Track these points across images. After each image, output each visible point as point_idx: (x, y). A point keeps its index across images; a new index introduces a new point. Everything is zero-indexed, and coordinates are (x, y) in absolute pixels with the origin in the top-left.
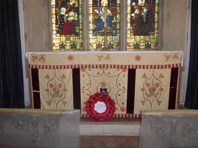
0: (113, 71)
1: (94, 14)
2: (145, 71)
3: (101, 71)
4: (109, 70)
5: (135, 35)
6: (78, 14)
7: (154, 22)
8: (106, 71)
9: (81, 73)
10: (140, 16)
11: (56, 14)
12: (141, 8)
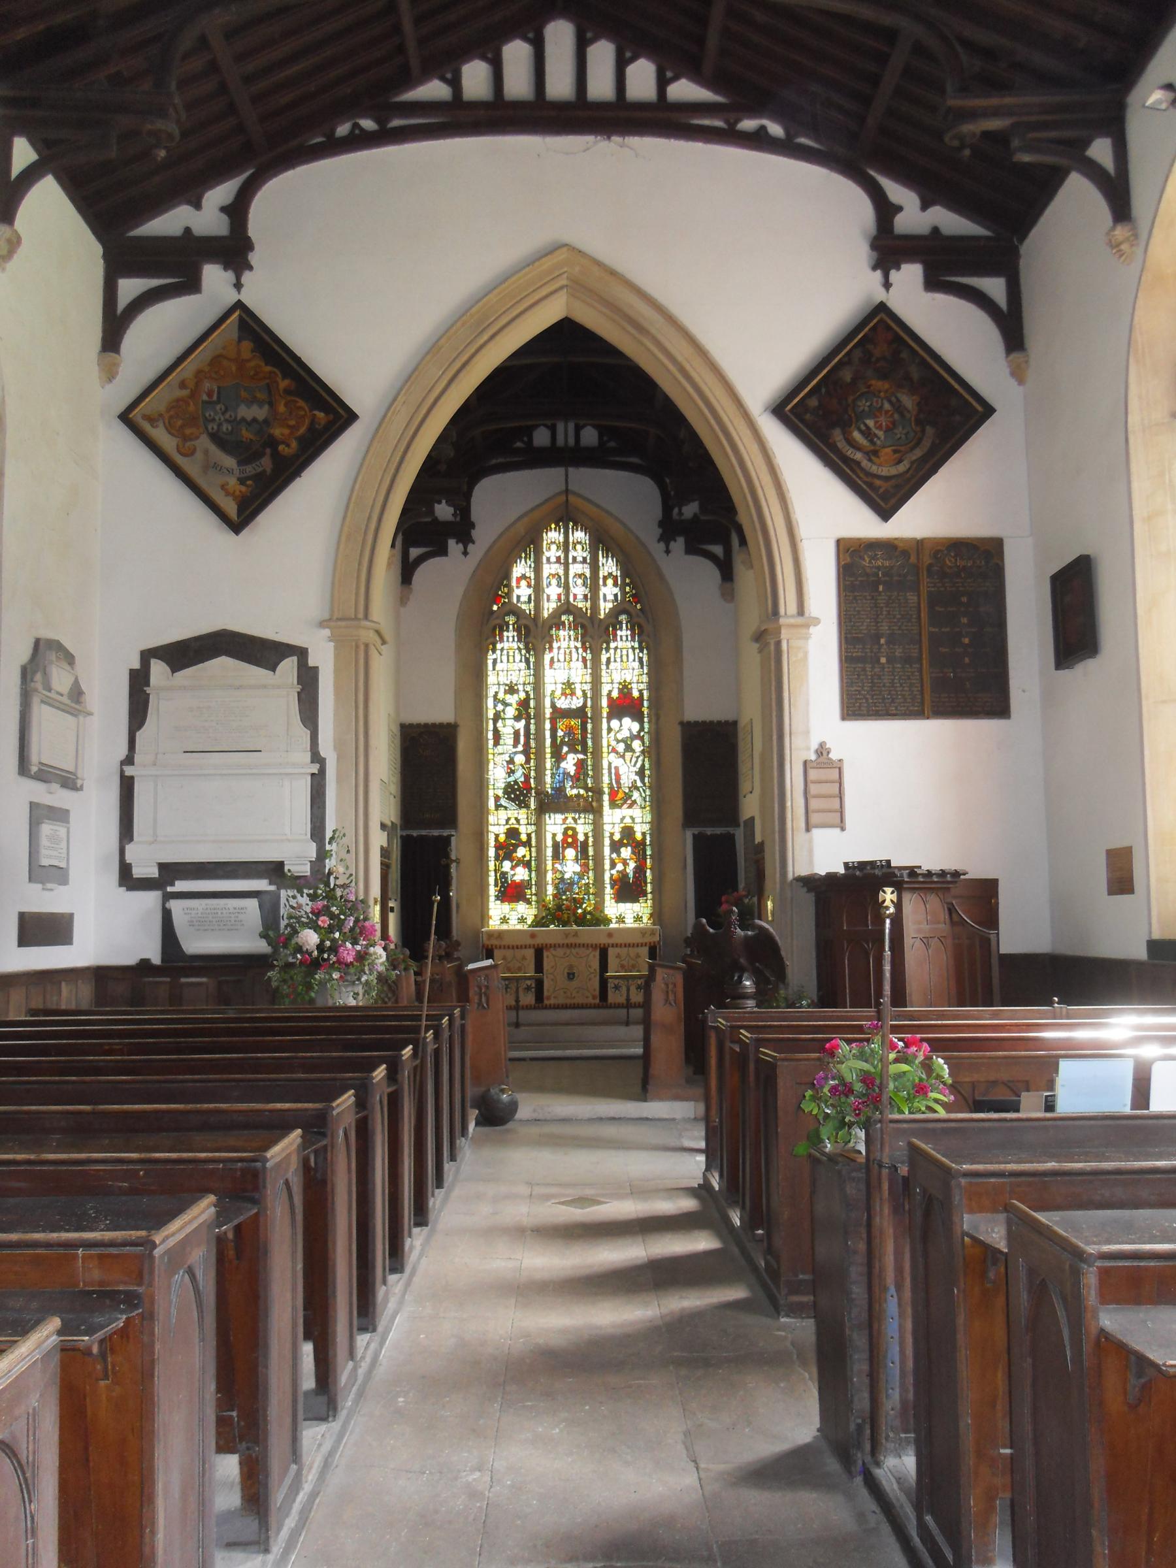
0: (581, 951)
1: (555, 870)
2: (618, 950)
3: (568, 951)
4: (577, 950)
5: (617, 902)
6: (530, 871)
7: (646, 883)
8: (574, 951)
9: (545, 954)
10: (624, 874)
11: (495, 871)
12: (625, 863)
